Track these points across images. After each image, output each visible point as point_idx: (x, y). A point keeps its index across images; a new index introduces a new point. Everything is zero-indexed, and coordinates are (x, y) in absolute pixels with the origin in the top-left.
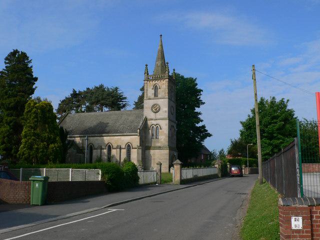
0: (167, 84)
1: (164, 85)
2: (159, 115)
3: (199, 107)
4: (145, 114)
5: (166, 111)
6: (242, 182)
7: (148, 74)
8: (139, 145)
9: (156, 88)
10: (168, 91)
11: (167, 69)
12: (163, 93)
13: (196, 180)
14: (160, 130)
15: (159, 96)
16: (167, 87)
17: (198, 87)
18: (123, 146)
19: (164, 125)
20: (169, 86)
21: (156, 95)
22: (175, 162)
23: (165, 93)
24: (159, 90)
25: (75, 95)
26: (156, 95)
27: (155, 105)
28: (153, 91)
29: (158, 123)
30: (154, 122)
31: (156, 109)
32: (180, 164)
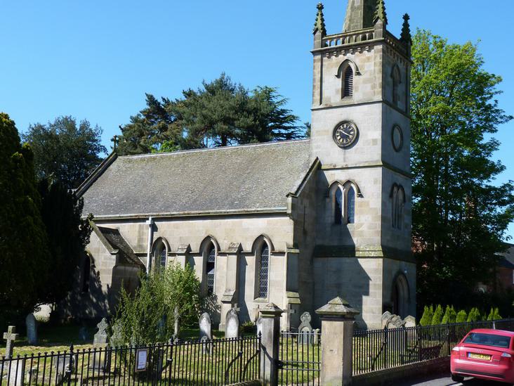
0: (379, 60)
1: (369, 64)
2: (354, 156)
3: (493, 131)
4: (314, 151)
5: (375, 141)
6: (130, 161)
7: (324, 33)
8: (291, 243)
9: (346, 73)
10: (384, 78)
11: (381, 15)
12: (369, 86)
13: (359, 191)
14: (357, 199)
15: (357, 96)
16: (379, 68)
17: (485, 69)
18: (248, 247)
19: (371, 185)
20: (384, 65)
21: (346, 92)
22: (325, 309)
23: (374, 87)
24: (355, 79)
25: (157, 110)
26: (346, 92)
27: (342, 123)
28: (339, 83)
29: (351, 178)
30: (341, 176)
31: (346, 135)
32: (495, 166)
